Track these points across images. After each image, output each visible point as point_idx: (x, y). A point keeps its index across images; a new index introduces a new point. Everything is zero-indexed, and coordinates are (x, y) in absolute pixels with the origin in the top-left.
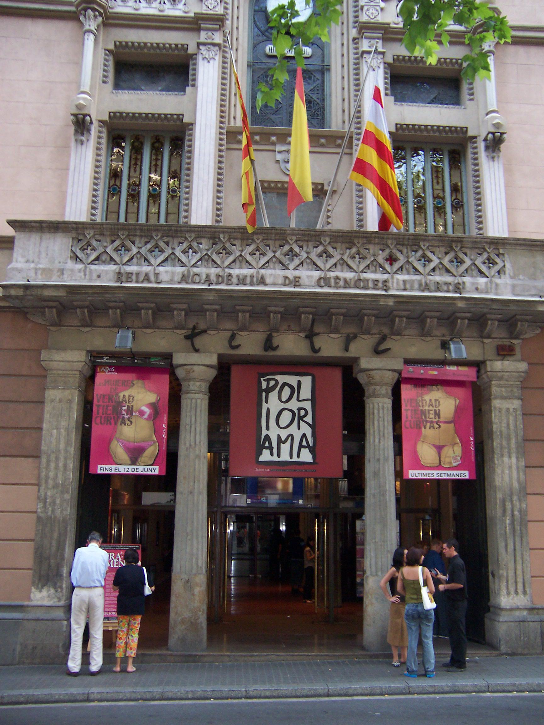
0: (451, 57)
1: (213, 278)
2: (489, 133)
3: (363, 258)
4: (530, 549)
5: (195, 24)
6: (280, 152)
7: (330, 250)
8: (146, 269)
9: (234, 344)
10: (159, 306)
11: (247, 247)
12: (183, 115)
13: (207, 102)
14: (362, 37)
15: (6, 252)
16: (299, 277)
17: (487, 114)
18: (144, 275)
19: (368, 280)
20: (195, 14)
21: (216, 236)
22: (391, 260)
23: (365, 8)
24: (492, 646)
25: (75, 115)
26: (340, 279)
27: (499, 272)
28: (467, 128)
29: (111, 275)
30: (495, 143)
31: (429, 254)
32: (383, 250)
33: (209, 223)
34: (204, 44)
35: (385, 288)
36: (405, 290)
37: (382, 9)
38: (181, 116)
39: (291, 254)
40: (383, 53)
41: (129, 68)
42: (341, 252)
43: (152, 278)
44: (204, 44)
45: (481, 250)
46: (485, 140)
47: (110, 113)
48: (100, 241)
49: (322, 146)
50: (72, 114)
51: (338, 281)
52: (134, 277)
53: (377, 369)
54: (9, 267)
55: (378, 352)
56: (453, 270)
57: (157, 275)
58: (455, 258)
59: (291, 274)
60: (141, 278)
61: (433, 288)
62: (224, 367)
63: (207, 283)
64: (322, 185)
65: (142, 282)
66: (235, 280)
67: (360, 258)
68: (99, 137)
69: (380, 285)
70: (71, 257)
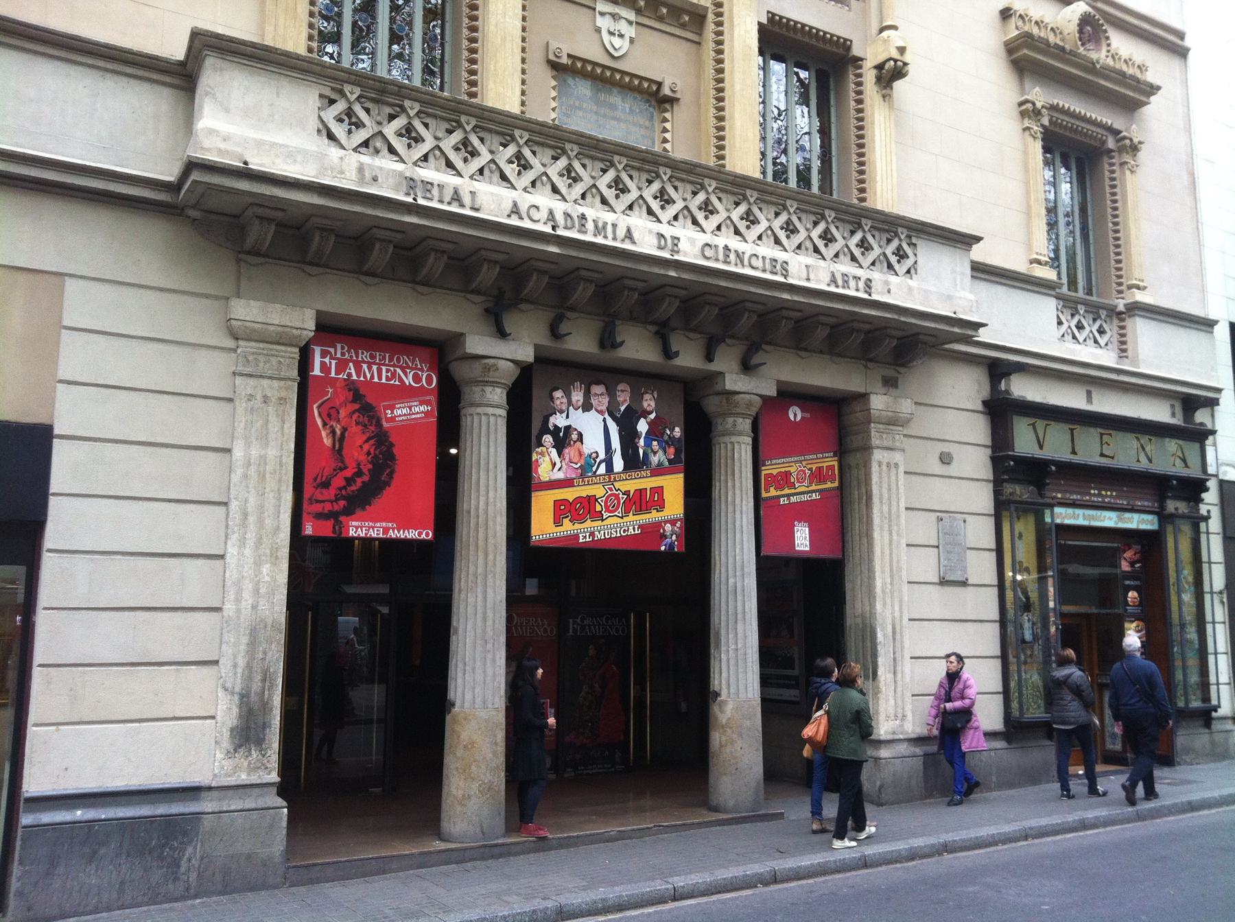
0: (827, 30)
1: (560, 218)
2: (891, 59)
4: (213, 717)
6: (602, 14)
16: (678, 239)
18: (452, 192)
21: (1059, 274)
27: (908, 272)
30: (891, 74)
31: (475, 141)
43: (467, 200)
49: (661, 19)
52: (435, 191)
55: (747, 367)
56: (459, 164)
59: (781, 256)
60: (447, 198)
61: (840, 282)
63: (550, 224)
64: (660, 84)
69: (778, 267)
70: (319, 131)
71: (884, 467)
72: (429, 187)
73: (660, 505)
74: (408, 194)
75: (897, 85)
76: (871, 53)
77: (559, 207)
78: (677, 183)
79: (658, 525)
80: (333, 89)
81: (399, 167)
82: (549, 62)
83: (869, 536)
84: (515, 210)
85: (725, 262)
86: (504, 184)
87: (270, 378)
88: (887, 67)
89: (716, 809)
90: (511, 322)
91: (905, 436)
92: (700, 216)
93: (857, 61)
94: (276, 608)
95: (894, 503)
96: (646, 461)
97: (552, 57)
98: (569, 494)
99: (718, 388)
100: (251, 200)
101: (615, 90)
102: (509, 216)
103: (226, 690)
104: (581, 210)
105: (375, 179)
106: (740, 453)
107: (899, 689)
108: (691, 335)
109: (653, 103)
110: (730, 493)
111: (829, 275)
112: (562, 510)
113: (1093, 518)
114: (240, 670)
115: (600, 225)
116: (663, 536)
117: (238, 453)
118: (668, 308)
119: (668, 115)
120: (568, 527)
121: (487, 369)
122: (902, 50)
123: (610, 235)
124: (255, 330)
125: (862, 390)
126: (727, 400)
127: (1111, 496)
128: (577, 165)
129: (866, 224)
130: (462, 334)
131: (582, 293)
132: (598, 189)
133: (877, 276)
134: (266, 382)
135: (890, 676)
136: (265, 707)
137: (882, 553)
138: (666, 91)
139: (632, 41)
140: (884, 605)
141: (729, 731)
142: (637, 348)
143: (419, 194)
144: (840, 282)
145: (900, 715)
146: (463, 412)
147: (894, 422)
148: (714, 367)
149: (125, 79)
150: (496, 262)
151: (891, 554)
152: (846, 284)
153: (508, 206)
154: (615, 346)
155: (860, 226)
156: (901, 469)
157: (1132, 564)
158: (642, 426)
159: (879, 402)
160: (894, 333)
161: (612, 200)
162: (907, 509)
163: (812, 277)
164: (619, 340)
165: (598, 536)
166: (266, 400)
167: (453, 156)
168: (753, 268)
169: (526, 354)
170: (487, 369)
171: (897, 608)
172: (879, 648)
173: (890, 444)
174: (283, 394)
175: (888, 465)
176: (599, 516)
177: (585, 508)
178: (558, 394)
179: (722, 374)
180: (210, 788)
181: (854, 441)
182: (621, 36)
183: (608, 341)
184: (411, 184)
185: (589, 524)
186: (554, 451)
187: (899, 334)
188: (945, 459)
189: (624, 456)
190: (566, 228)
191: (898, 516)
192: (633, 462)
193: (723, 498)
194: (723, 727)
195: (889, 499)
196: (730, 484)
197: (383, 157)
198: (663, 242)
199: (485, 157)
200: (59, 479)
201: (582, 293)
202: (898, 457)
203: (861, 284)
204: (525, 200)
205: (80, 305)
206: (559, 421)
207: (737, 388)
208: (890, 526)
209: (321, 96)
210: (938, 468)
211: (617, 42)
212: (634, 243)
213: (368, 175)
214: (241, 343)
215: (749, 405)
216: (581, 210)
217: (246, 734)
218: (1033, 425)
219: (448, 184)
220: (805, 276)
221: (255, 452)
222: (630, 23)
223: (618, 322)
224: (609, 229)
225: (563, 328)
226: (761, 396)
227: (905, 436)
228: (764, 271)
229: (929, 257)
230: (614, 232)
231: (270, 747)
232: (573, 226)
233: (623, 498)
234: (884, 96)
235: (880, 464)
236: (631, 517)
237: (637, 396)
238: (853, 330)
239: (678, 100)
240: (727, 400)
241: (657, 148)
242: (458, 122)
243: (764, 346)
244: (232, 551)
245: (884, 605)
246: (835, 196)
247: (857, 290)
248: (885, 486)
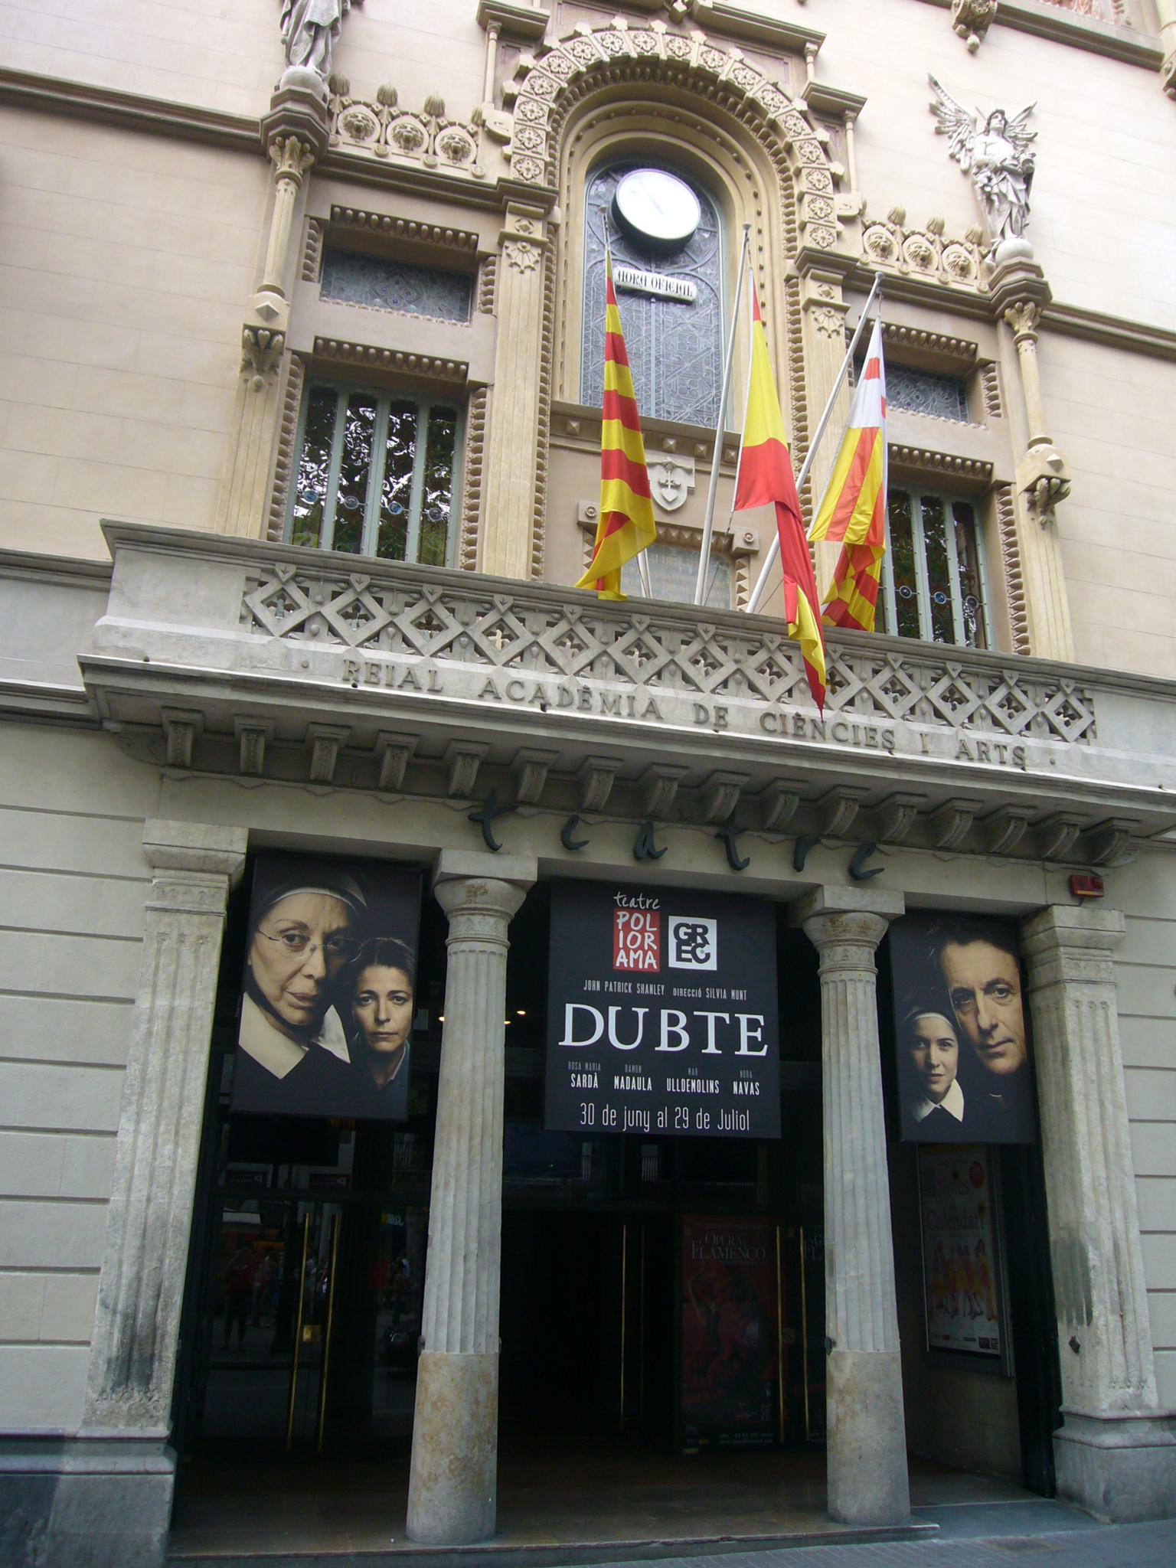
1: (552, 695)
3: (779, 675)
5: (491, 200)
7: (716, 651)
11: (407, 609)
12: (467, 364)
14: (804, 277)
15: (95, 597)
16: (726, 710)
17: (1030, 446)
18: (404, 673)
19: (783, 717)
20: (500, 180)
22: (953, 697)
23: (804, 172)
25: (254, 330)
26: (803, 720)
27: (1083, 735)
28: (467, 364)
29: (754, 721)
30: (1048, 496)
32: (1050, 697)
33: (255, 537)
34: (515, 239)
35: (888, 745)
36: (925, 752)
37: (839, 234)
38: (463, 367)
39: (953, 697)
40: (844, 310)
41: (349, 253)
42: (604, 639)
43: (425, 680)
44: (515, 239)
45: (485, 607)
46: (1031, 489)
47: (317, 338)
50: (246, 327)
51: (800, 723)
53: (852, 907)
54: (99, 623)
55: (857, 877)
57: (722, 712)
58: (770, 666)
60: (399, 681)
61: (975, 754)
63: (538, 703)
64: (731, 537)
65: (644, 716)
67: (573, 646)
68: (291, 384)
69: (879, 738)
70: (242, 618)
71: (1085, 1009)
72: (374, 670)
74: (346, 680)
75: (1058, 507)
76: (1019, 471)
77: (551, 680)
78: (1025, 688)
80: (263, 570)
81: (341, 649)
82: (580, 524)
83: (1067, 1106)
84: (964, 752)
85: (796, 736)
86: (260, 630)
87: (189, 912)
88: (1038, 487)
89: (835, 1519)
91: (1115, 962)
92: (945, 708)
93: (1002, 487)
94: (178, 1198)
95: (1104, 1059)
97: (583, 519)
99: (817, 906)
100: (160, 703)
101: (673, 550)
102: (481, 696)
103: (107, 1307)
104: (583, 682)
105: (305, 667)
106: (855, 995)
107: (1130, 1339)
108: (771, 837)
109: (726, 559)
110: (843, 1052)
111: (958, 745)
114: (124, 1281)
115: (611, 699)
117: (144, 1003)
118: (724, 802)
119: (742, 572)
121: (473, 892)
122: (1057, 465)
123: (625, 712)
124: (172, 855)
125: (1040, 901)
126: (833, 922)
128: (902, 676)
129: (1011, 678)
130: (439, 850)
131: (598, 789)
132: (609, 656)
133: (1032, 742)
134: (183, 918)
135: (1114, 1320)
137: (1090, 1133)
138: (738, 543)
139: (691, 492)
140: (1098, 1209)
141: (848, 1399)
142: (690, 858)
143: (362, 678)
144: (975, 754)
145: (1134, 1380)
146: (450, 949)
147: (1092, 945)
148: (809, 876)
149: (11, 583)
150: (473, 756)
151: (1104, 1135)
152: (984, 755)
153: (480, 686)
154: (653, 856)
155: (1002, 680)
156: (1113, 1011)
159: (1067, 917)
160: (1074, 819)
161: (1063, 730)
162: (1125, 1067)
163: (930, 748)
164: (658, 848)
167: (691, 670)
168: (840, 741)
169: (527, 870)
170: (473, 892)
171: (1118, 1214)
172: (1092, 1275)
173: (1092, 976)
174: (205, 931)
179: (819, 887)
180: (75, 1439)
181: (1042, 974)
182: (676, 487)
183: (645, 851)
184: (352, 668)
187: (1082, 821)
190: (561, 706)
191: (1113, 1078)
193: (834, 1059)
194: (840, 1392)
195: (1097, 1054)
196: (842, 1038)
197: (321, 641)
198: (702, 715)
199: (856, 685)
201: (598, 789)
202: (1105, 994)
203: (1008, 755)
207: (843, 906)
208: (1100, 1093)
209: (248, 579)
211: (671, 495)
212: (659, 718)
213: (295, 663)
214: (157, 872)
215: (864, 928)
216: (583, 682)
217: (130, 1365)
219: (400, 665)
220: (920, 748)
221: (162, 1002)
222: (689, 472)
223: (657, 825)
224: (624, 702)
225: (579, 834)
226: (883, 915)
227: (1115, 962)
228: (857, 744)
229: (1109, 713)
230: (631, 706)
231: (158, 1388)
232: (571, 703)
234: (1043, 525)
235: (1078, 1004)
238: (1010, 818)
239: (755, 553)
240: (833, 922)
241: (734, 607)
242: (420, 593)
243: (882, 847)
244: (126, 1125)
245: (1098, 1209)
246: (990, 649)
247: (1003, 763)
248: (1088, 1034)
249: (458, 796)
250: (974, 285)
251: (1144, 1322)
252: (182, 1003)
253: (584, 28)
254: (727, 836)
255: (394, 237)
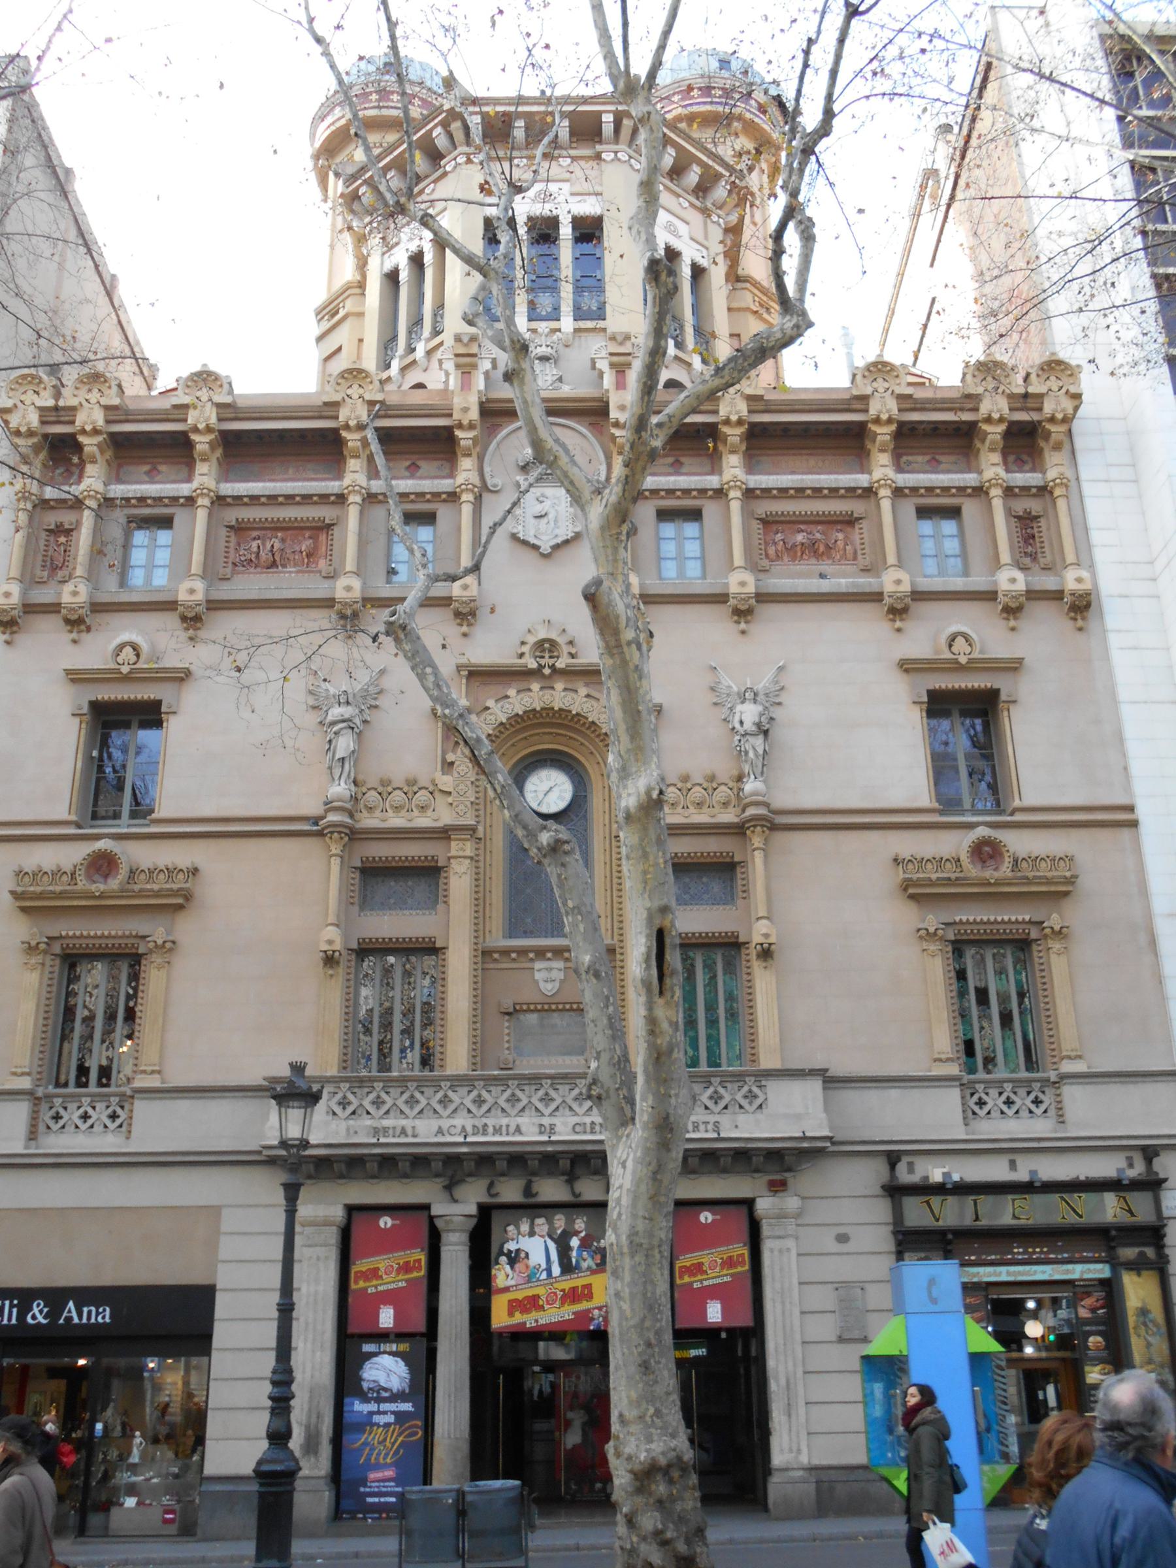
1: (469, 1129)
5: (444, 834)
8: (403, 1122)
9: (493, 1191)
10: (418, 1163)
13: (458, 920)
24: (766, 1509)
43: (410, 1132)
44: (455, 857)
48: (70, 577)
62: (485, 1213)
66: (491, 1130)
73: (590, 1296)
79: (589, 1311)
90: (459, 1192)
96: (578, 1267)
98: (520, 1295)
107: (794, 1429)
112: (515, 1306)
113: (1068, 1272)
116: (593, 1319)
120: (518, 1318)
127: (1041, 1252)
135: (784, 1419)
136: (318, 1434)
147: (782, 1216)
157: (1093, 1310)
158: (575, 1242)
165: (541, 1322)
166: (318, 1259)
170: (447, 1222)
171: (790, 1364)
173: (781, 1233)
175: (780, 1251)
176: (542, 1308)
177: (533, 1303)
178: (511, 1228)
185: (534, 1315)
186: (508, 1267)
188: (843, 1238)
189: (561, 1264)
192: (567, 1268)
200: (219, 1312)
202: (790, 1243)
203: (710, 1127)
204: (445, 1124)
205: (230, 1221)
206: (511, 1246)
210: (835, 1247)
211: (549, 986)
216: (484, 1120)
218: (928, 1202)
233: (560, 1294)
235: (772, 1251)
236: (566, 1307)
237: (570, 1221)
249: (437, 1175)
250: (729, 817)
251: (802, 1419)
252: (321, 1288)
253: (490, 703)
254: (571, 1178)
255: (392, 872)
